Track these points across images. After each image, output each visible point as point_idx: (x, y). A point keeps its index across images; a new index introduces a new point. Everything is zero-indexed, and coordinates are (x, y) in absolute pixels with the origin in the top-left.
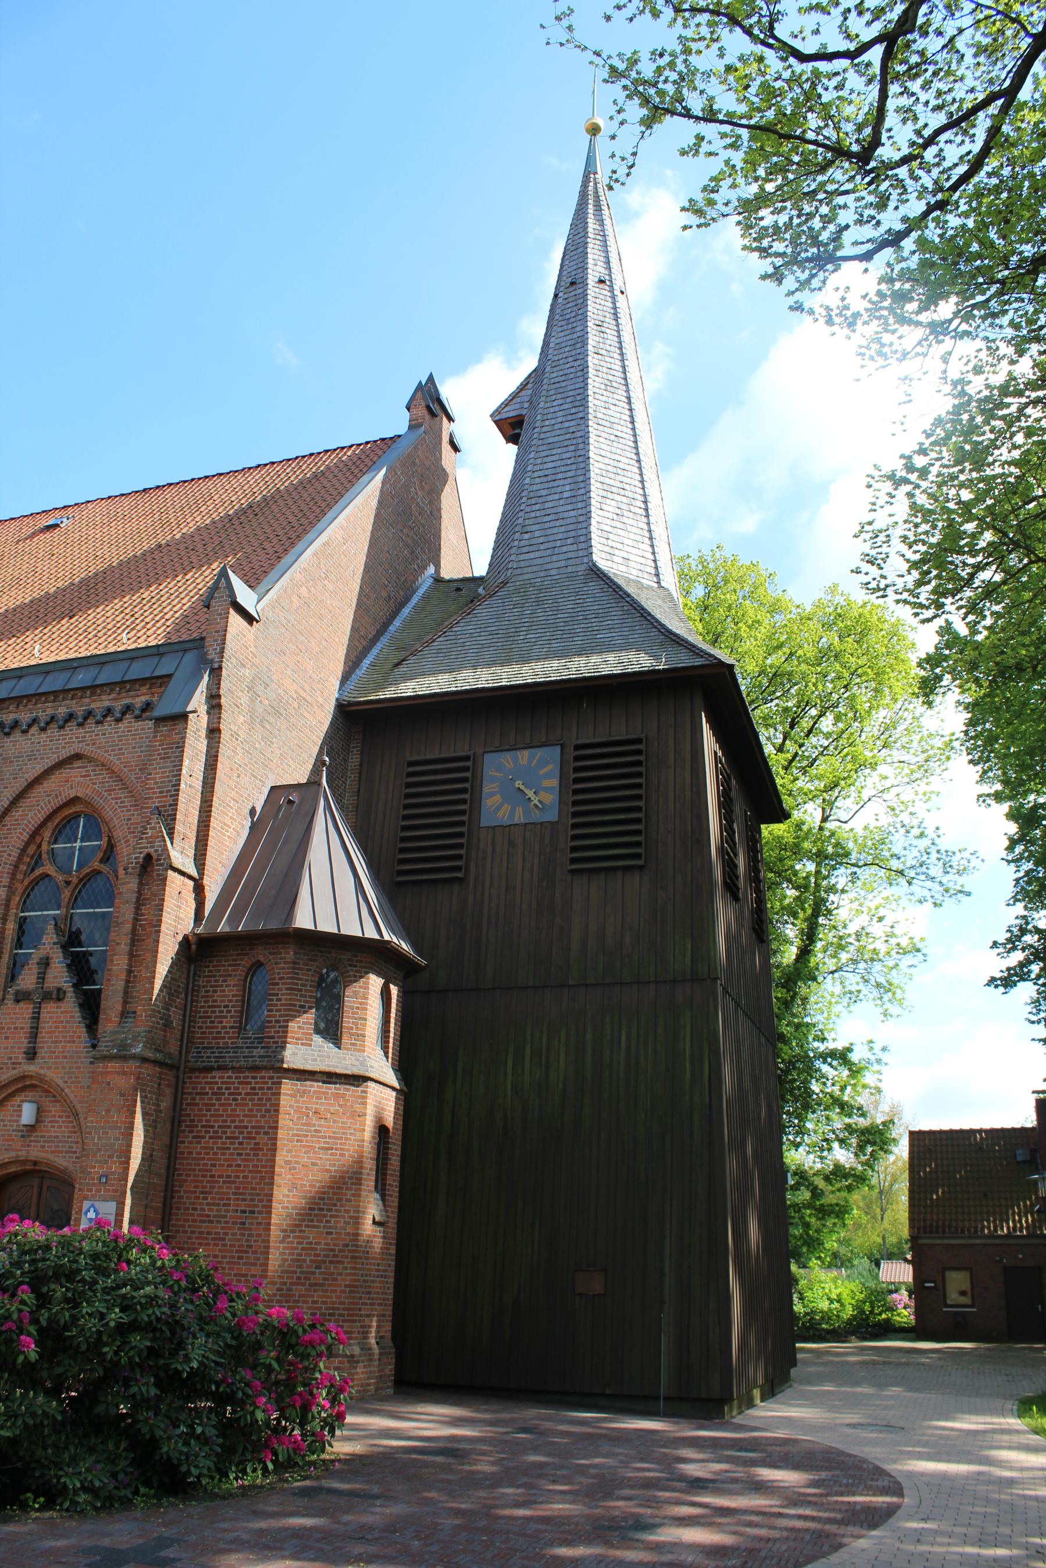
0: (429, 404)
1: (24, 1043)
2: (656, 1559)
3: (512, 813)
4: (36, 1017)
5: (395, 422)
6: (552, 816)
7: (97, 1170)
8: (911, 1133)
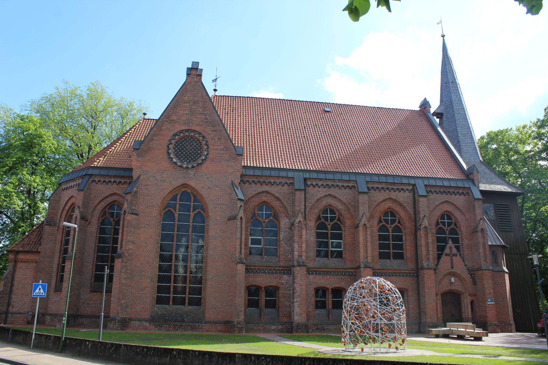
1: (450, 265)
2: (433, 354)
4: (452, 260)
6: (492, 205)
7: (488, 292)
8: (380, 258)
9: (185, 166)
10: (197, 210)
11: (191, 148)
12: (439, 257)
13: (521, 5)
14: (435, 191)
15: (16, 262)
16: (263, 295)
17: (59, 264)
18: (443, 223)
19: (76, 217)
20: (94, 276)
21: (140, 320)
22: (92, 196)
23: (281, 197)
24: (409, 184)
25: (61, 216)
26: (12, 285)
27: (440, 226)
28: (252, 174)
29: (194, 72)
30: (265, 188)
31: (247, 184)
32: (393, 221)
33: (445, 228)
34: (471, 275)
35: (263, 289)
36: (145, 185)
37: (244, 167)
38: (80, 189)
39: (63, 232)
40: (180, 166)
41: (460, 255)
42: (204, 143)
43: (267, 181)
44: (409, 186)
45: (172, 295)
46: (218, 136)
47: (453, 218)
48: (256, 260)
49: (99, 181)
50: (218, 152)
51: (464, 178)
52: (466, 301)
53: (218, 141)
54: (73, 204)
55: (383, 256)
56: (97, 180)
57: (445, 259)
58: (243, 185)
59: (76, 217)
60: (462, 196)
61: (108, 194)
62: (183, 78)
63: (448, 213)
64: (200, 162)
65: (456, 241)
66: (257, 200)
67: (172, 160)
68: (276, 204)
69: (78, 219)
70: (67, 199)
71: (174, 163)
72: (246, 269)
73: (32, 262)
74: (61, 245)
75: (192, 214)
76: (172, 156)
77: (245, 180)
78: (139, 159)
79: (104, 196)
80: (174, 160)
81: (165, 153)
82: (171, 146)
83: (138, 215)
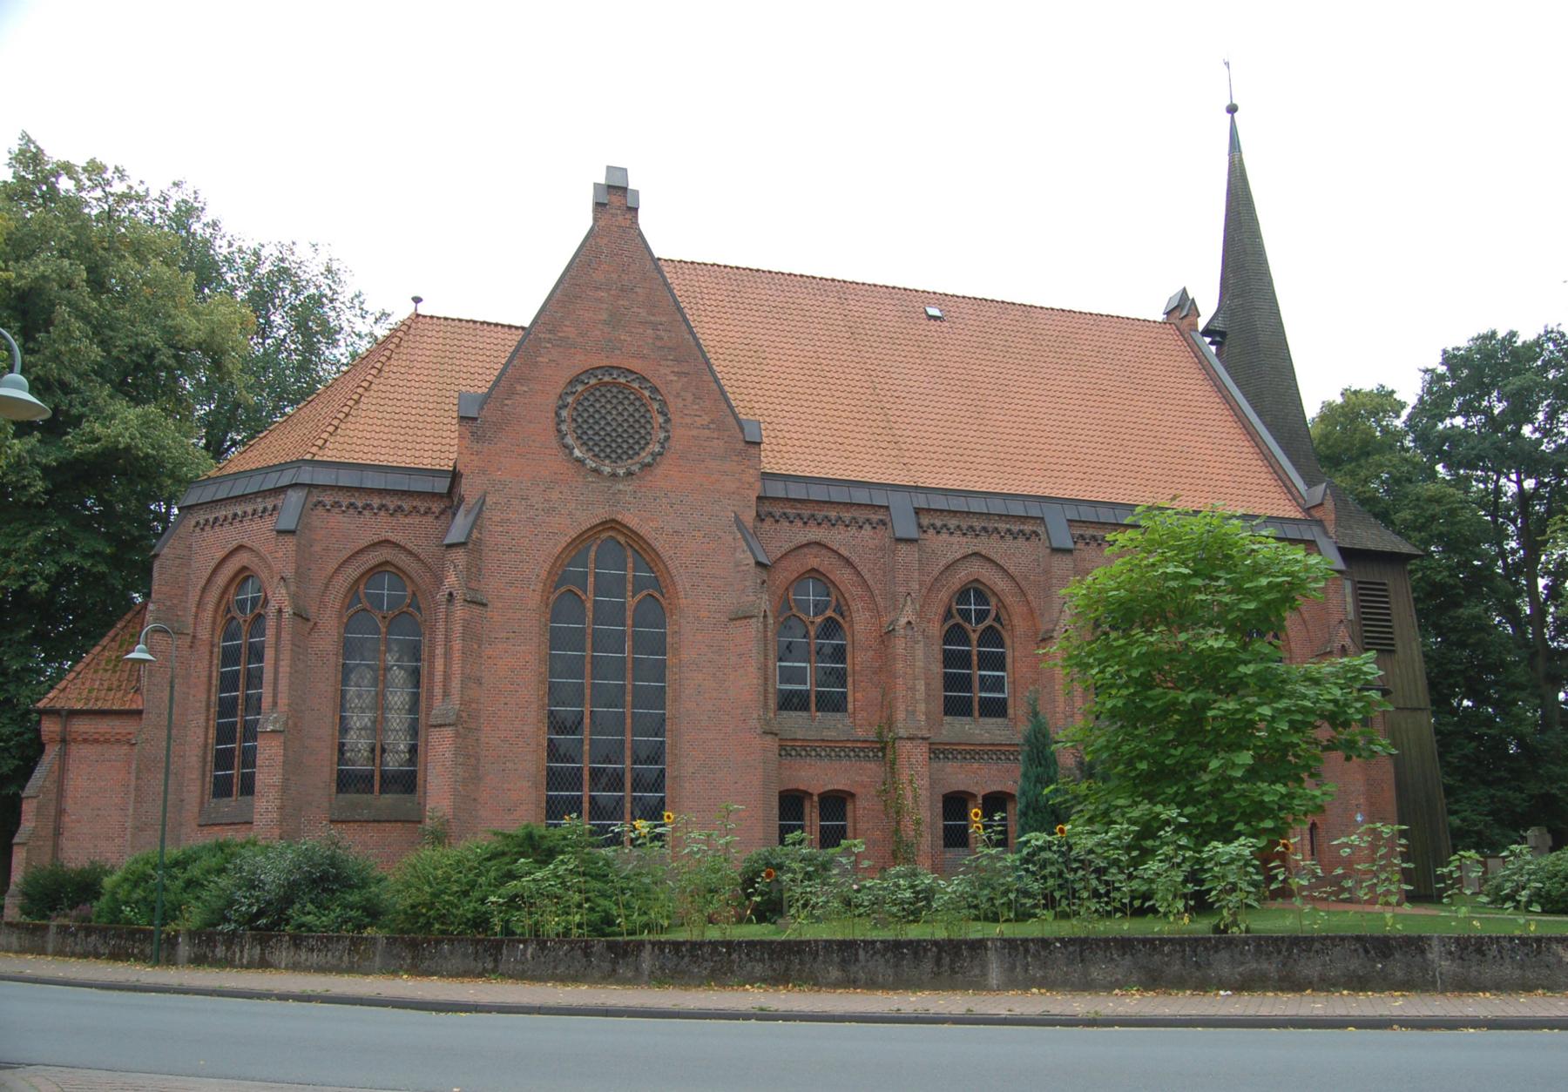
10: (645, 592)
11: (620, 419)
14: (799, 516)
15: (63, 741)
16: (975, 813)
17: (206, 745)
19: (280, 611)
22: (317, 548)
23: (855, 559)
25: (199, 604)
26: (60, 812)
28: (782, 494)
29: (615, 202)
30: (814, 534)
31: (769, 521)
32: (982, 616)
35: (816, 798)
37: (766, 476)
38: (282, 527)
39: (212, 652)
42: (656, 406)
43: (820, 515)
48: (797, 724)
49: (337, 504)
50: (695, 432)
51: (1299, 516)
54: (244, 568)
55: (956, 707)
59: (280, 611)
63: (975, 585)
64: (648, 459)
66: (794, 567)
67: (571, 453)
68: (842, 576)
70: (220, 555)
71: (578, 460)
73: (118, 741)
74: (209, 691)
75: (631, 602)
77: (925, 521)
78: (476, 447)
80: (577, 453)
82: (564, 413)
83: (485, 605)
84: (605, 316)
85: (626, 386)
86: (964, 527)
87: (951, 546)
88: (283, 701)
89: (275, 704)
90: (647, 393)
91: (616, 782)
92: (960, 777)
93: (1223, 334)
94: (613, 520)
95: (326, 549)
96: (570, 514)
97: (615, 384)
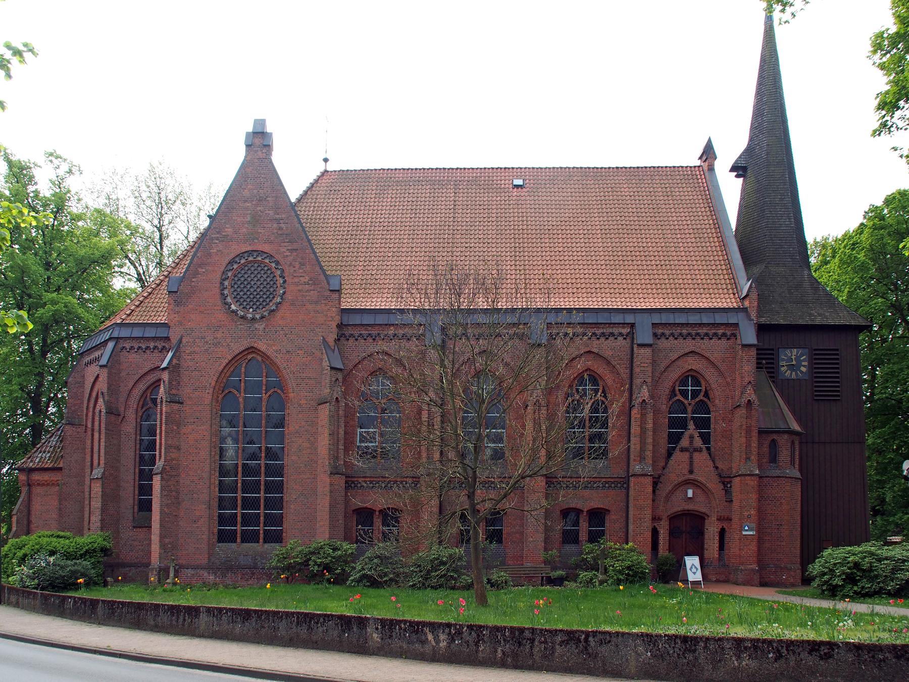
0: (709, 153)
1: (687, 467)
3: (804, 366)
4: (691, 458)
5: (692, 159)
9: (251, 316)
10: (272, 390)
12: (669, 454)
13: (205, 180)
15: (29, 485)
18: (684, 393)
19: (100, 411)
20: (136, 502)
21: (195, 568)
22: (123, 374)
24: (624, 324)
27: (677, 398)
29: (259, 142)
31: (351, 340)
33: (686, 402)
34: (725, 485)
35: (585, 514)
36: (190, 354)
40: (242, 317)
41: (708, 449)
42: (279, 272)
44: (624, 328)
45: (239, 528)
46: (299, 260)
47: (703, 383)
50: (300, 288)
52: (712, 530)
53: (300, 268)
56: (128, 346)
57: (679, 457)
58: (345, 342)
59: (100, 411)
60: (724, 342)
61: (146, 369)
62: (237, 155)
64: (274, 307)
65: (703, 423)
69: (103, 414)
70: (92, 380)
71: (233, 311)
72: (346, 482)
73: (53, 484)
76: (229, 300)
78: (177, 309)
79: (142, 372)
80: (233, 307)
81: (218, 296)
83: (182, 403)
84: (249, 219)
85: (262, 262)
86: (729, 333)
87: (674, 347)
88: (102, 462)
89: (99, 464)
90: (273, 265)
91: (247, 503)
92: (567, 498)
93: (744, 169)
94: (252, 347)
95: (128, 374)
96: (228, 345)
97: (255, 262)
